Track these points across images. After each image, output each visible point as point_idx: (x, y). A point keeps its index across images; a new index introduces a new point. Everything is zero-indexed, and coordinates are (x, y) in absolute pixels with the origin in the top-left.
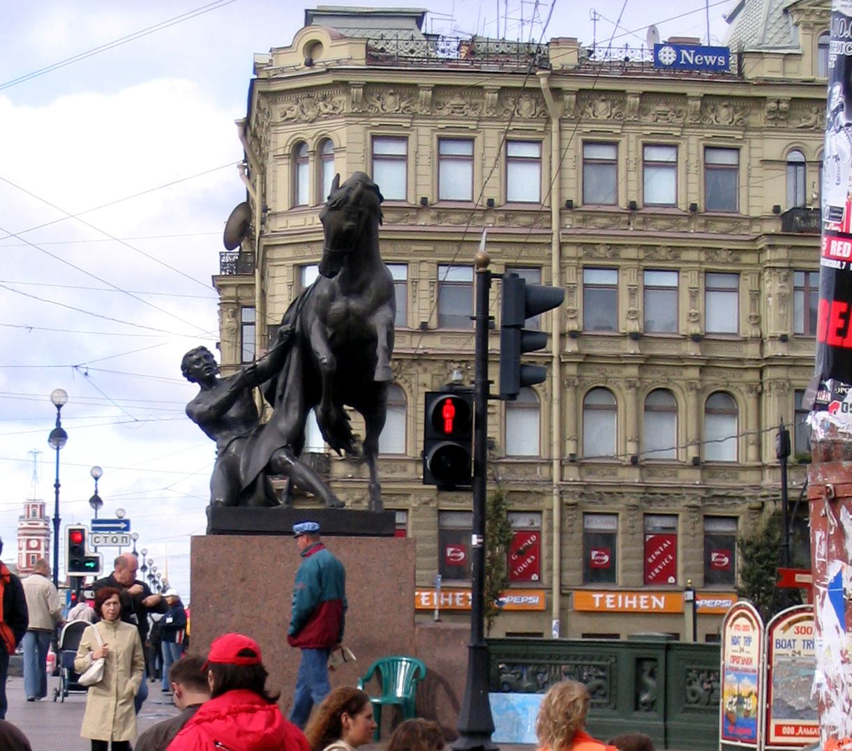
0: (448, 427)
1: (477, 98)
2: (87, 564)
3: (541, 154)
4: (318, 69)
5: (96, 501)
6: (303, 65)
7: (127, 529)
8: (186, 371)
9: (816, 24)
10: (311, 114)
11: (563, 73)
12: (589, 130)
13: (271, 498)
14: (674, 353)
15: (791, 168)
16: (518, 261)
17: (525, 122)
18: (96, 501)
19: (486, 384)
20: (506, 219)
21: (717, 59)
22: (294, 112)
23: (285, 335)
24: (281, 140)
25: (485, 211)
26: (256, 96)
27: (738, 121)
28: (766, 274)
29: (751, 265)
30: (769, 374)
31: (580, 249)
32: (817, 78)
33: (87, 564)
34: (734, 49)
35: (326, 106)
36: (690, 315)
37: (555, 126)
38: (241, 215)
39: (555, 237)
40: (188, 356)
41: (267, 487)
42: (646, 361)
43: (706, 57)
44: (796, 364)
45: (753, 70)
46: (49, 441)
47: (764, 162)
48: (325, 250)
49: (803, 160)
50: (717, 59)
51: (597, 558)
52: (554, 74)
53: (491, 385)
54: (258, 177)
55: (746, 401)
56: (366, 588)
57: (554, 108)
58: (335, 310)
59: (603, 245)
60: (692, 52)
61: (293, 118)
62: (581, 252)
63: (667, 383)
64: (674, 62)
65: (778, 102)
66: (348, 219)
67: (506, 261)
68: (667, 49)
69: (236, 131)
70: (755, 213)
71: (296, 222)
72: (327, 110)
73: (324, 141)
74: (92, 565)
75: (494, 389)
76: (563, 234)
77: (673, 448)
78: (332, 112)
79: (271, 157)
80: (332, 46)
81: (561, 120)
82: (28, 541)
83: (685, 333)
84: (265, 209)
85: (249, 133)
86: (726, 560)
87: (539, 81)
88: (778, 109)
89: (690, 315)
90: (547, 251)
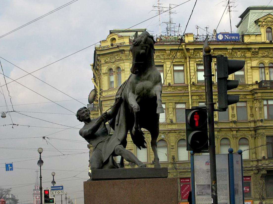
0: (197, 124)
1: (164, 53)
2: (50, 201)
3: (184, 69)
4: (114, 46)
5: (54, 182)
6: (110, 46)
7: (62, 189)
8: (78, 117)
9: (265, 25)
10: (113, 60)
11: (190, 44)
12: (198, 61)
13: (114, 165)
14: (228, 127)
15: (260, 69)
16: (180, 101)
17: (178, 59)
18: (54, 182)
19: (212, 105)
20: (174, 89)
21: (235, 37)
22: (108, 60)
23: (118, 100)
24: (104, 69)
25: (168, 87)
26: (96, 56)
27: (243, 55)
28: (255, 102)
29: (250, 99)
30: (259, 131)
31: (197, 97)
32: (266, 41)
33: (50, 201)
34: (240, 34)
35: (118, 58)
36: (232, 115)
37: (188, 60)
38: (93, 93)
39: (190, 94)
40: (79, 111)
41: (114, 162)
42: (219, 130)
43: (232, 37)
44: (266, 128)
45: (247, 40)
46: (38, 164)
47: (252, 67)
48: (133, 63)
49: (264, 66)
50: (235, 37)
51: (245, 190)
52: (186, 44)
53: (215, 105)
54: (98, 81)
55: (251, 140)
56: (157, 200)
57: (188, 54)
58: (137, 87)
59: (242, 95)
60: (228, 35)
61: (108, 62)
62: (198, 98)
63: (226, 136)
64: (222, 39)
65: (255, 49)
66: (142, 49)
67: (175, 101)
68: (220, 35)
69: (91, 67)
70: (250, 83)
71: (111, 93)
72: (118, 59)
73: (118, 68)
74: (52, 201)
75: (216, 106)
76: (192, 92)
77: (248, 150)
78: (119, 59)
79: (102, 74)
80: (118, 39)
81: (189, 57)
82: (36, 197)
83: (231, 121)
84: (101, 90)
85: (95, 68)
86: (248, 190)
87: (182, 47)
88: (255, 51)
89: (232, 115)
90: (187, 98)
